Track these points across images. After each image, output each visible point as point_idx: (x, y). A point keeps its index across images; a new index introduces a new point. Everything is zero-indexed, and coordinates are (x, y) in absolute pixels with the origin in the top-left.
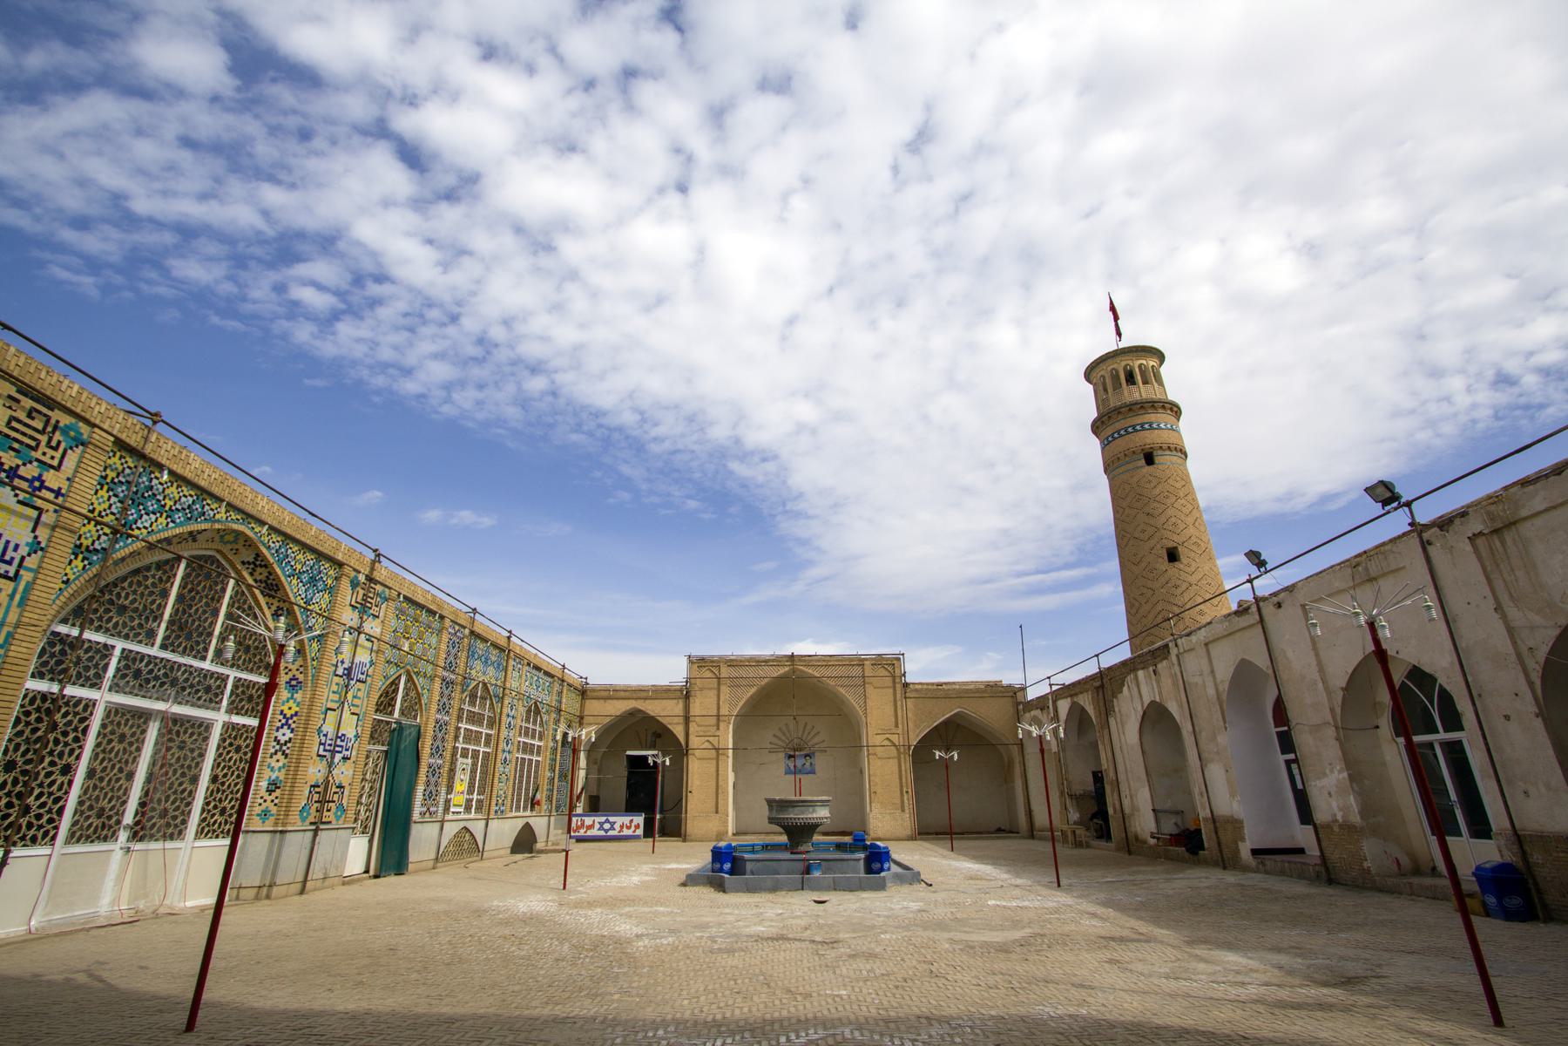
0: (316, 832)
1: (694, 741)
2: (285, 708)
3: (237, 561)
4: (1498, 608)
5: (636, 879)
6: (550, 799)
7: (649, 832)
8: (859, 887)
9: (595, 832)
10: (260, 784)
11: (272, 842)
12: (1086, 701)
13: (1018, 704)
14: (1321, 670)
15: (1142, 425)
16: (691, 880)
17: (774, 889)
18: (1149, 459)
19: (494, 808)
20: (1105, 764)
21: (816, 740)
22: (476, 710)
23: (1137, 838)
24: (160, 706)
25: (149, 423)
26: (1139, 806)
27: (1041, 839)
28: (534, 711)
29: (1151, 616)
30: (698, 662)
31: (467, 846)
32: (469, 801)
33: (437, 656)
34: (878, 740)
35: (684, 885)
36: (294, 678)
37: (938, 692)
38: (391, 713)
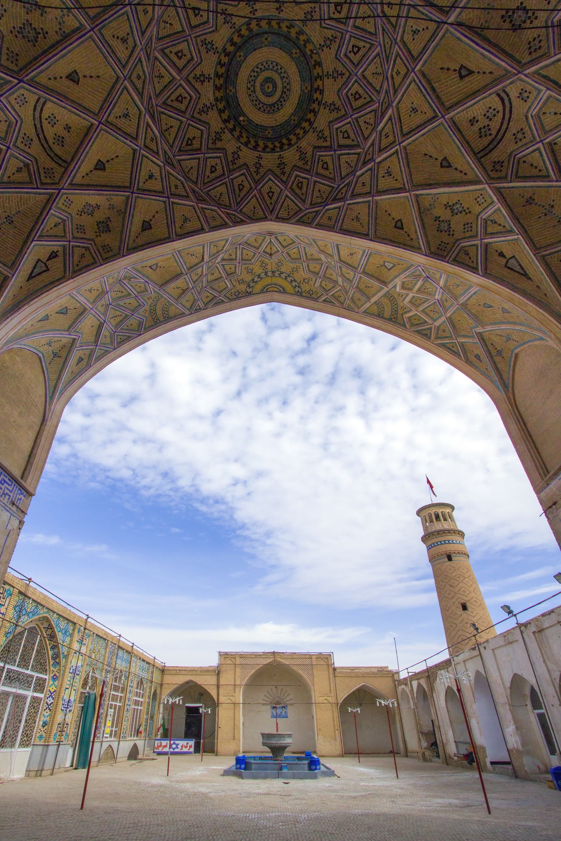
0: (59, 745)
1: (222, 699)
2: (51, 688)
3: (42, 627)
4: (544, 662)
5: (198, 773)
6: (145, 730)
7: (197, 749)
8: (304, 777)
9: (166, 749)
10: (39, 723)
11: (43, 750)
12: (423, 682)
13: (394, 681)
14: (502, 679)
15: (445, 541)
16: (226, 773)
17: (265, 777)
18: (450, 558)
19: (122, 735)
20: (434, 718)
21: (287, 699)
22: (117, 684)
23: (450, 757)
24: (14, 690)
25: (28, 582)
26: (449, 738)
27: (413, 757)
28: (141, 683)
29: (456, 638)
30: (224, 655)
31: (111, 755)
32: (112, 731)
33: (104, 659)
34: (321, 700)
35: (223, 775)
36: (55, 675)
37: (353, 673)
38: (86, 689)
